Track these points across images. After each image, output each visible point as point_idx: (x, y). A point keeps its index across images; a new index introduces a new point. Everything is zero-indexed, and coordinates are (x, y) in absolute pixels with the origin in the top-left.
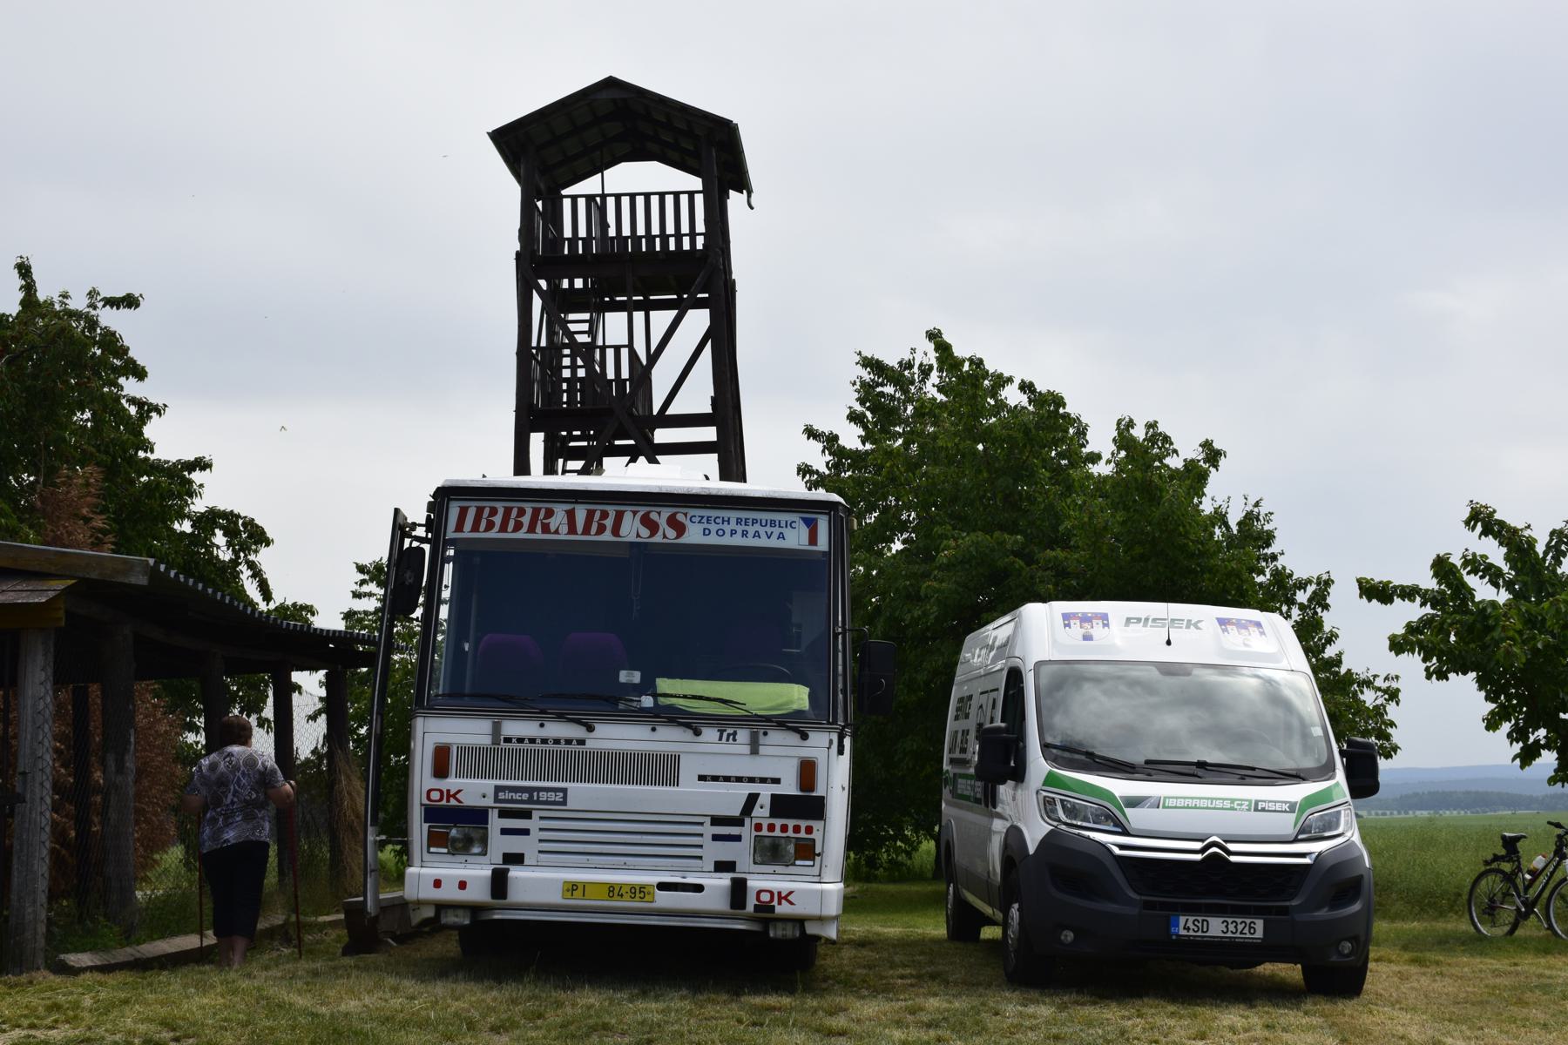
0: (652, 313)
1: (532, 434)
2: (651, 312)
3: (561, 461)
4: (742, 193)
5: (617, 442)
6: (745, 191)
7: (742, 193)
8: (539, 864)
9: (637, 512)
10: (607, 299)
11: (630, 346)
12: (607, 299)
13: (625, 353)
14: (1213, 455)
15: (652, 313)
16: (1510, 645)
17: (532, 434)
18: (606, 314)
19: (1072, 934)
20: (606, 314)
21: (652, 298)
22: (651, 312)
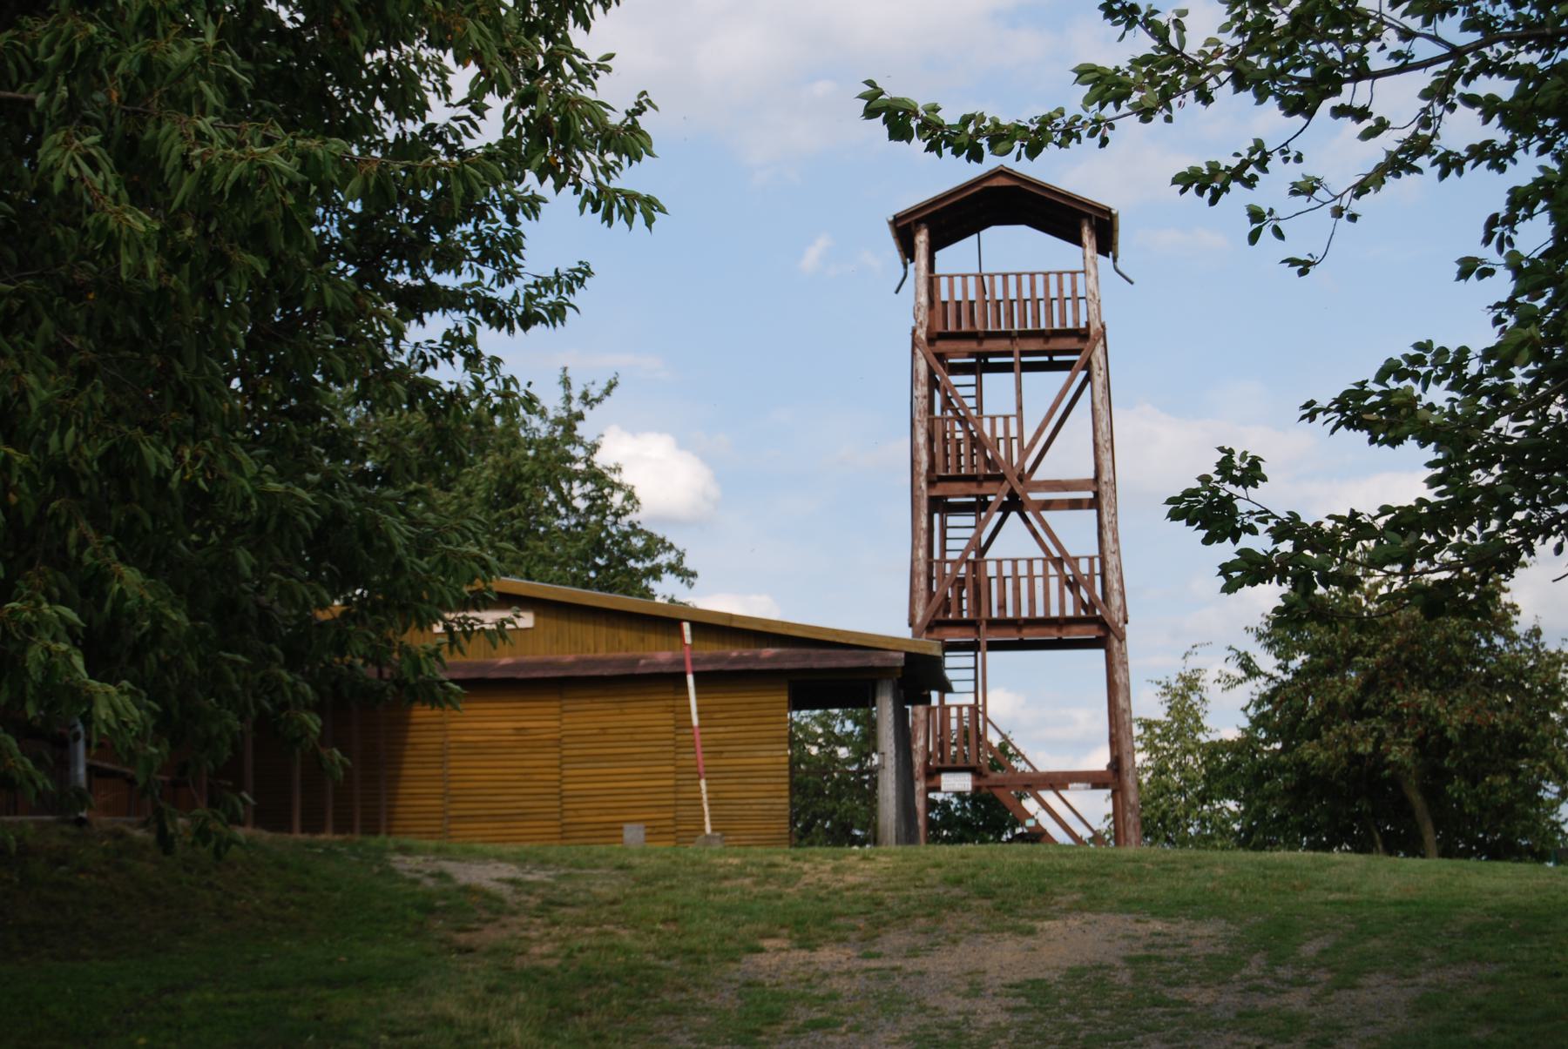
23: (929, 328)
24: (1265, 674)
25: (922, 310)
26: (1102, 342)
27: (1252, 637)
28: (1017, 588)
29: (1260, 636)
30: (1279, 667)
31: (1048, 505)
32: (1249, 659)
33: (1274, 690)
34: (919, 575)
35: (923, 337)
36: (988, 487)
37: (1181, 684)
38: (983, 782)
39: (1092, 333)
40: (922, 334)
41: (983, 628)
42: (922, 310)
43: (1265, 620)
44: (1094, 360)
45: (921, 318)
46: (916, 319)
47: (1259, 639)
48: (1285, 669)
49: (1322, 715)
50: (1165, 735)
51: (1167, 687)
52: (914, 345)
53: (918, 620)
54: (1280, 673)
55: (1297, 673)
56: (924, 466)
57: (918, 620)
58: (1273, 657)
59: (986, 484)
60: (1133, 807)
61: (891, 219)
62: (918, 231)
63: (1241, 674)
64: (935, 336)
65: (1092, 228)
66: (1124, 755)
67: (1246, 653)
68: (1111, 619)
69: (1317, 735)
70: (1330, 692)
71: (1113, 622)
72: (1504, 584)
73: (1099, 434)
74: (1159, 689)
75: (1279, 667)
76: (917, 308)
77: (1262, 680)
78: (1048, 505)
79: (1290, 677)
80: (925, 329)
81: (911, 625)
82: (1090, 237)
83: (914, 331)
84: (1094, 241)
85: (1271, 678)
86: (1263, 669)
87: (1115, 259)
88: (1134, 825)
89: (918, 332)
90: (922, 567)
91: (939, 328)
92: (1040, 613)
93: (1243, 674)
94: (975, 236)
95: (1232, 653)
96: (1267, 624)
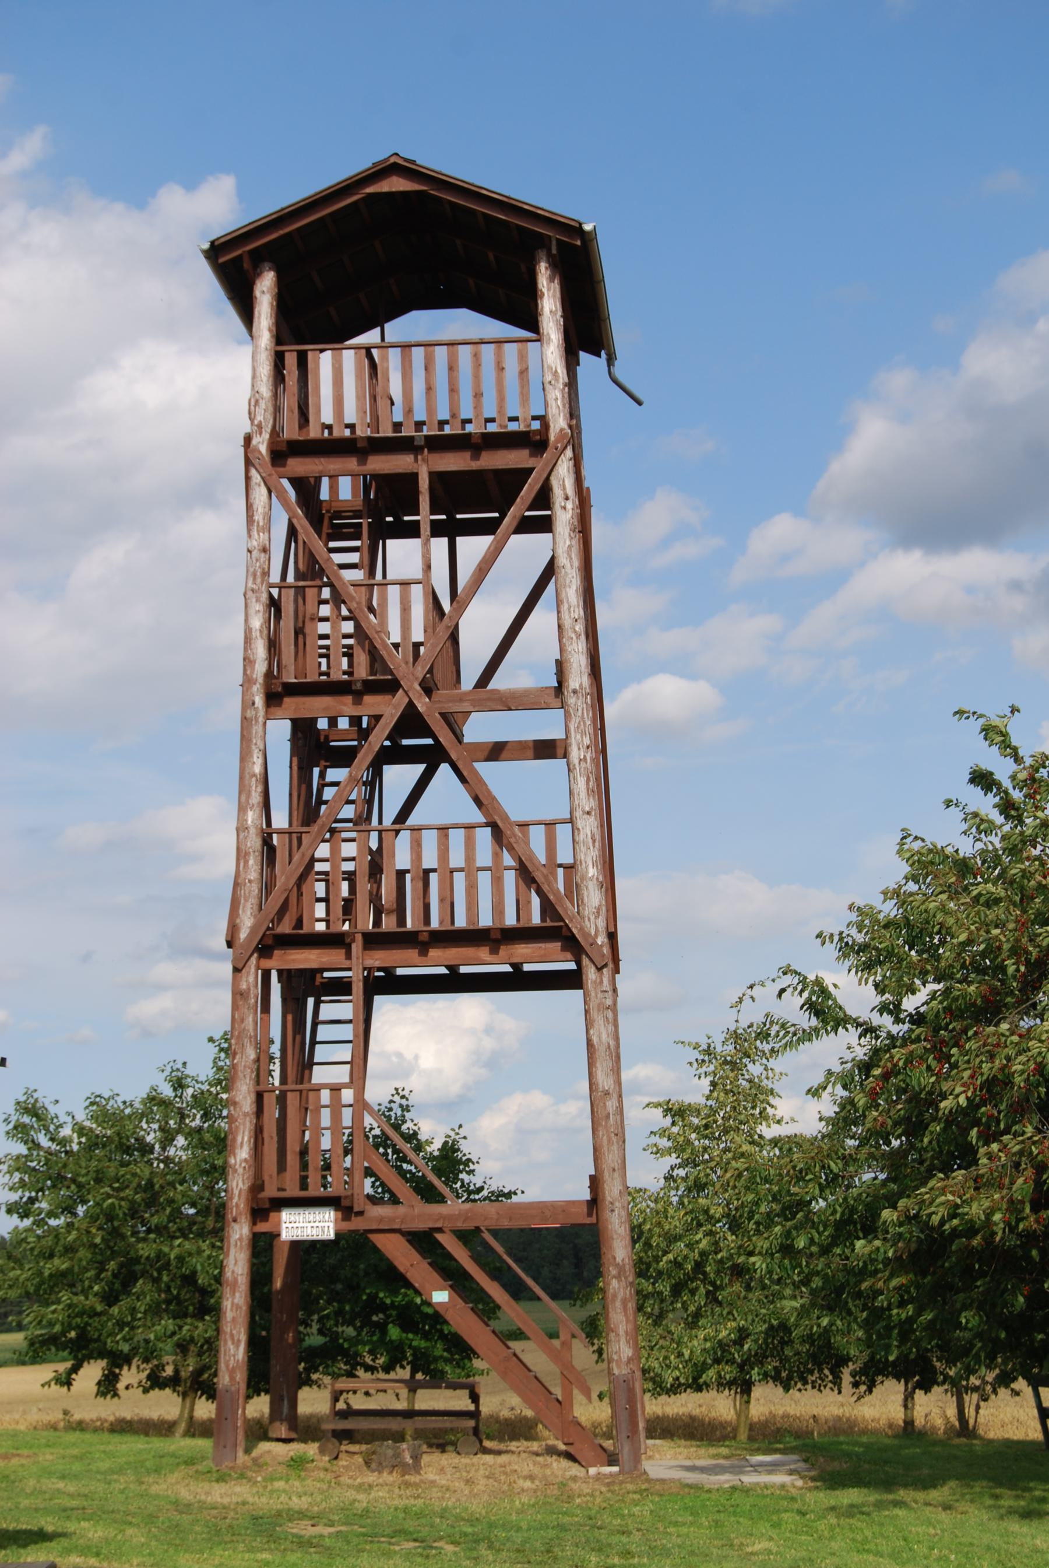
0: (460, 540)
1: (376, 997)
2: (458, 539)
3: (316, 771)
4: (599, 356)
5: (405, 742)
6: (603, 353)
7: (599, 356)
8: (578, 678)
9: (395, 1200)
10: (389, 519)
11: (426, 581)
12: (389, 519)
13: (417, 593)
14: (851, 907)
15: (460, 540)
16: (32, 1127)
17: (376, 997)
18: (388, 542)
19: (820, 1284)
20: (388, 542)
21: (458, 516)
22: (458, 539)
23: (275, 433)
24: (857, 1024)
25: (263, 404)
26: (569, 452)
27: (831, 950)
28: (448, 888)
29: (847, 948)
30: (883, 1009)
31: (496, 751)
32: (824, 992)
33: (876, 1052)
34: (247, 854)
35: (263, 449)
36: (373, 703)
37: (730, 1048)
38: (357, 1224)
39: (552, 437)
40: (262, 444)
41: (357, 947)
42: (263, 404)
43: (853, 917)
44: (554, 482)
45: (259, 418)
46: (252, 420)
47: (846, 956)
48: (893, 1010)
49: (973, 1105)
50: (706, 1126)
51: (708, 1051)
52: (248, 463)
53: (243, 935)
54: (886, 1022)
55: (918, 1019)
56: (260, 668)
57: (243, 935)
58: (870, 987)
59: (368, 699)
60: (621, 1269)
61: (206, 246)
62: (257, 274)
63: (807, 1021)
64: (284, 447)
65: (554, 265)
66: (606, 1174)
67: (818, 982)
68: (581, 929)
69: (968, 1157)
70: (992, 1057)
71: (587, 935)
72: (673, 1160)
73: (565, 607)
74: (696, 1055)
75: (883, 1009)
76: (254, 402)
77: (850, 1036)
78: (496, 751)
79: (906, 1027)
80: (266, 436)
81: (230, 944)
82: (551, 279)
83: (248, 439)
84: (556, 285)
85: (868, 1030)
86: (852, 1011)
87: (611, 360)
88: (624, 1302)
89: (254, 442)
90: (254, 842)
91: (290, 432)
92: (461, 922)
93: (814, 1022)
94: (378, 330)
95: (788, 980)
96: (860, 928)
